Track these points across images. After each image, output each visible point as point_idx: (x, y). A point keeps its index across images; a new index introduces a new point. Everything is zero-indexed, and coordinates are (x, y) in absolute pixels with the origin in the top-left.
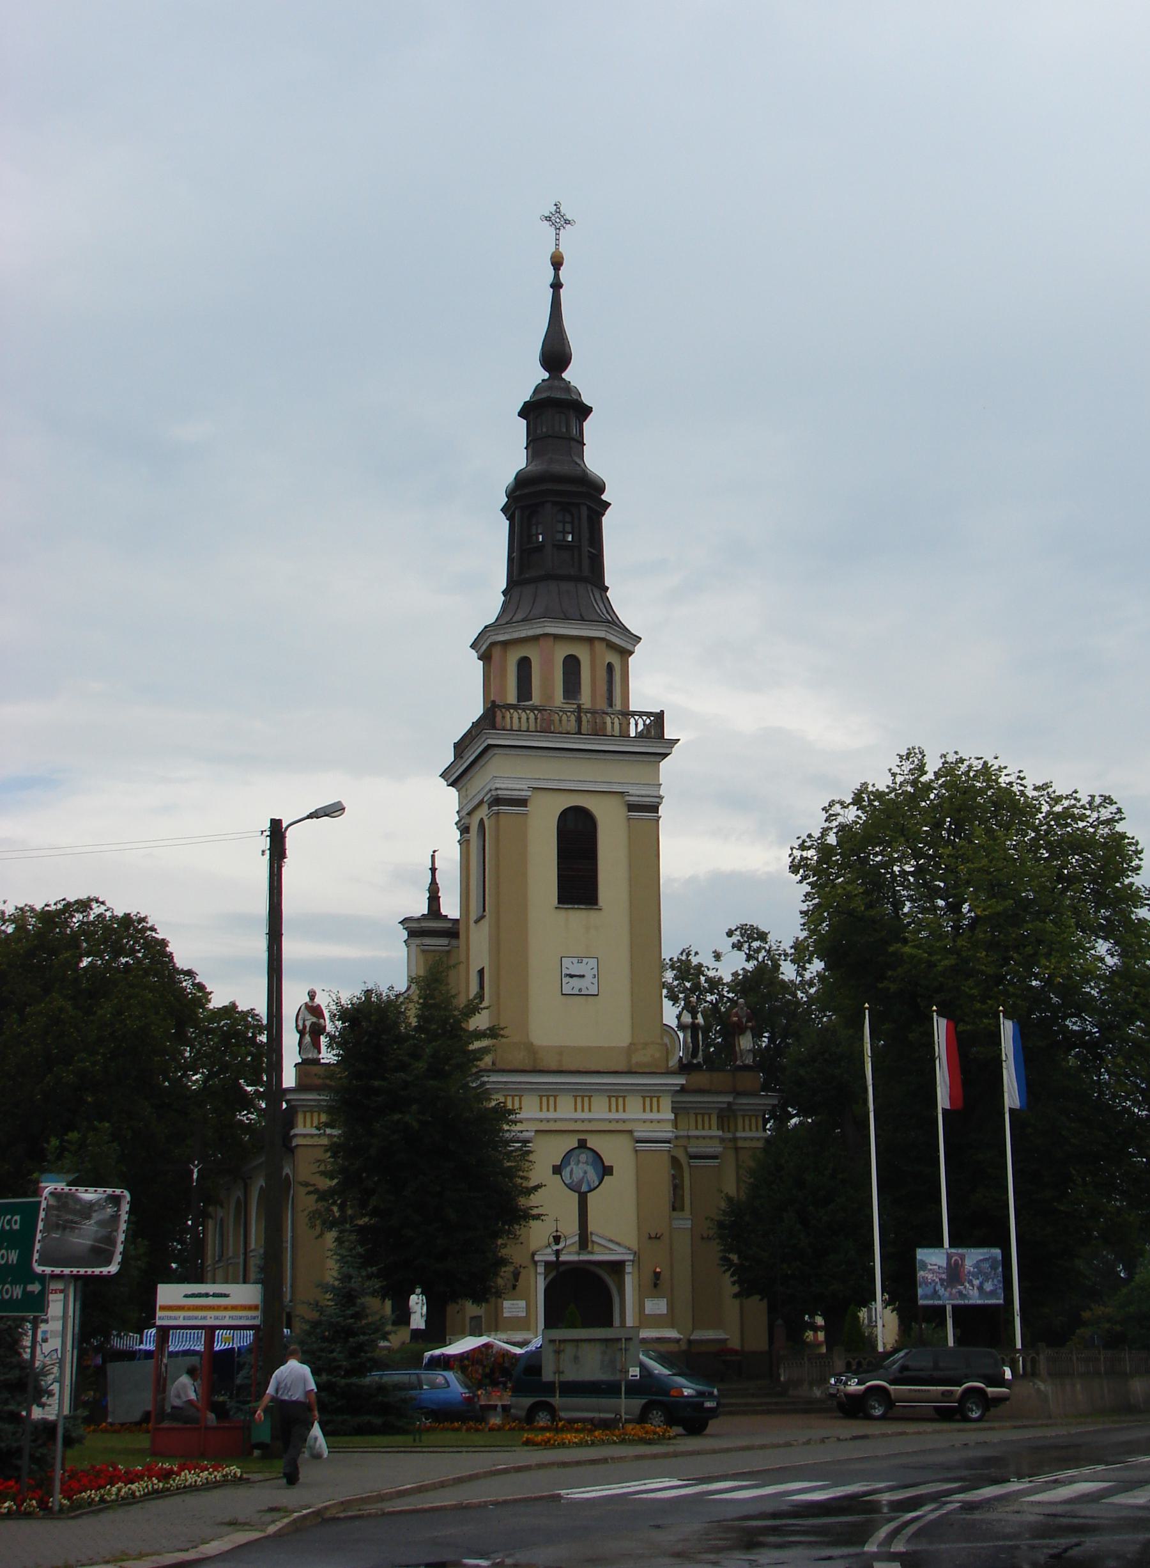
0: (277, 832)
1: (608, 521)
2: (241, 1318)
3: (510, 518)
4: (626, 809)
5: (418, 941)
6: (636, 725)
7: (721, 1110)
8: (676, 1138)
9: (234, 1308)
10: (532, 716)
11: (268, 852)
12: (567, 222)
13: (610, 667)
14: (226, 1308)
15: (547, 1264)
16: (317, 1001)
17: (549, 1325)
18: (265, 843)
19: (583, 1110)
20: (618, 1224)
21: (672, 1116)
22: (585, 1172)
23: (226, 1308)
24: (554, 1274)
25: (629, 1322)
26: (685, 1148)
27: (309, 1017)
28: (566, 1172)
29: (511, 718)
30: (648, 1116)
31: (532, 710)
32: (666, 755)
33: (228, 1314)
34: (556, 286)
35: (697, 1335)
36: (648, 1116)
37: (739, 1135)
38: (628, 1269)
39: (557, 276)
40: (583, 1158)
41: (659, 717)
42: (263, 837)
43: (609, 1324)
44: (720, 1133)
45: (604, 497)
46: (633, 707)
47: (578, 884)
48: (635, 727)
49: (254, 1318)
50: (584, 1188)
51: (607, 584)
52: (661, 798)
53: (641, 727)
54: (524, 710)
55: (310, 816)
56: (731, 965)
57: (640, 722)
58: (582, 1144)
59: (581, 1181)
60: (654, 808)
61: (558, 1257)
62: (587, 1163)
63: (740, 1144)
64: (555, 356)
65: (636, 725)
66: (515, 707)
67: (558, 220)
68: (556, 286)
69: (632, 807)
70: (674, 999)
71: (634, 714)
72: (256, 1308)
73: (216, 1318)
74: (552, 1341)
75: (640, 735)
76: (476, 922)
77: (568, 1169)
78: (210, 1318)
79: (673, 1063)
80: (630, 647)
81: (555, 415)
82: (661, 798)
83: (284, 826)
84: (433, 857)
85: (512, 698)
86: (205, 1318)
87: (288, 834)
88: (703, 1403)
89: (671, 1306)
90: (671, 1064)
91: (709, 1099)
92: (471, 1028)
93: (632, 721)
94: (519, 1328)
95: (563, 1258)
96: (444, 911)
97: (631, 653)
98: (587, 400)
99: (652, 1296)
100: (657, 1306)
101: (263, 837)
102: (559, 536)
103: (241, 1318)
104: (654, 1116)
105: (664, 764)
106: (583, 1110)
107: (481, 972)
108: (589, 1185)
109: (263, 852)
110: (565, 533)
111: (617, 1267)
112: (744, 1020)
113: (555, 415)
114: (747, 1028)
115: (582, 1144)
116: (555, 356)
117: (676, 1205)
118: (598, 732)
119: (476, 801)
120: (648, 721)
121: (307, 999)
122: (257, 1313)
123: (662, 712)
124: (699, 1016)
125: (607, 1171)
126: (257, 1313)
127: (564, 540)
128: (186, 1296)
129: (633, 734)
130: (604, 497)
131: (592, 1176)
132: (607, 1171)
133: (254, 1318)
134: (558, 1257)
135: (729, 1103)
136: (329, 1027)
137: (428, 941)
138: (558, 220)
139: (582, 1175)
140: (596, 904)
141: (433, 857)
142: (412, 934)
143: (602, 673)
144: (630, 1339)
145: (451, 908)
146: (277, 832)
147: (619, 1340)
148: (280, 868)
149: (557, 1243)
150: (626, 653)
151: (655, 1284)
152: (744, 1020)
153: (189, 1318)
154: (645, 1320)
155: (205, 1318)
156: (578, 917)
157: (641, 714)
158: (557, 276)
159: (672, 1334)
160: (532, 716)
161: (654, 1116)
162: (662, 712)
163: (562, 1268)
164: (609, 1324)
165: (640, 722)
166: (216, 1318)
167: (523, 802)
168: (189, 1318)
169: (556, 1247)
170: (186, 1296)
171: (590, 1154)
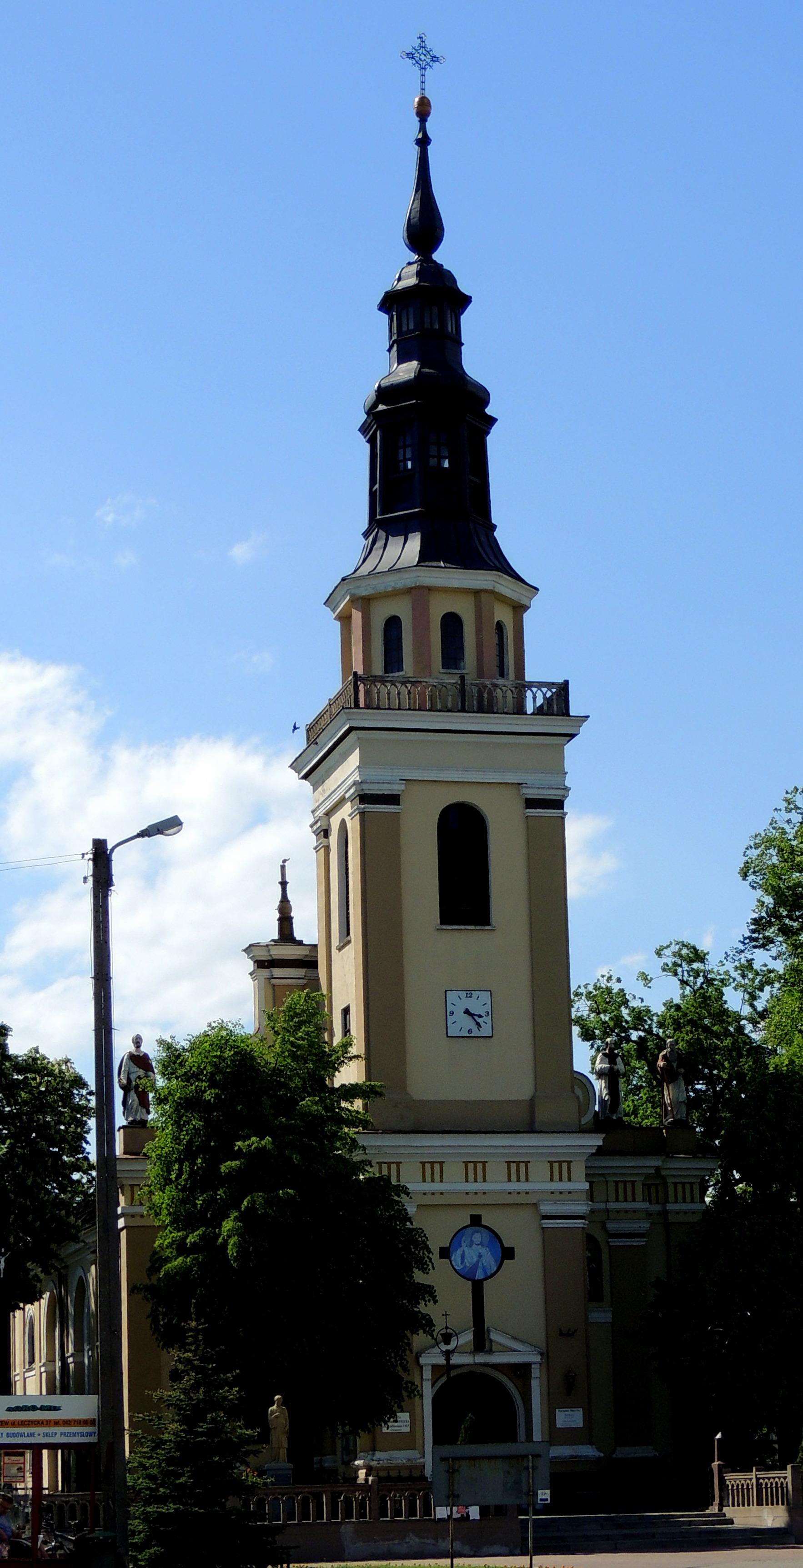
0: (101, 855)
1: (494, 441)
2: (74, 1435)
3: (372, 441)
4: (522, 804)
5: (265, 973)
6: (534, 698)
7: (648, 1176)
8: (592, 1212)
9: (67, 1423)
10: (404, 691)
11: (91, 879)
12: (435, 59)
13: (500, 627)
14: (57, 1423)
15: (435, 1367)
16: (144, 1049)
17: (438, 1440)
18: (88, 868)
19: (433, 1181)
20: (518, 1339)
21: (586, 1186)
22: (480, 1256)
23: (57, 1423)
24: (444, 1379)
25: (537, 1437)
26: (603, 1224)
27: (135, 1069)
28: (456, 1257)
29: (379, 693)
30: (556, 1186)
31: (403, 683)
32: (572, 736)
33: (59, 1430)
34: (423, 142)
35: (624, 1452)
36: (556, 1186)
37: (669, 1207)
38: (536, 1372)
39: (423, 129)
40: (477, 1238)
41: (563, 689)
42: (85, 861)
43: (513, 1439)
44: (645, 1205)
45: (489, 411)
46: (528, 678)
47: (465, 898)
48: (533, 700)
49: (91, 1434)
50: (479, 1275)
51: (494, 521)
52: (567, 789)
53: (540, 701)
54: (393, 683)
55: (143, 834)
56: (661, 994)
57: (540, 696)
58: (476, 1220)
59: (475, 1267)
60: (558, 804)
61: (448, 1359)
62: (481, 1244)
63: (672, 1218)
64: (425, 230)
65: (534, 698)
66: (383, 681)
67: (422, 57)
68: (423, 142)
69: (531, 803)
70: (588, 1035)
71: (531, 685)
72: (92, 1422)
73: (47, 1435)
74: (443, 1459)
75: (539, 711)
76: (340, 949)
77: (459, 1252)
78: (39, 1436)
79: (587, 1119)
80: (524, 601)
81: (427, 312)
82: (567, 789)
83: (109, 847)
84: (283, 868)
85: (378, 668)
86: (32, 1435)
87: (114, 856)
88: (426, 556)
89: (588, 1418)
90: (583, 1121)
91: (633, 1164)
92: (337, 1085)
93: (529, 694)
94: (409, 1435)
95: (456, 1360)
96: (298, 935)
97: (525, 608)
98: (464, 286)
99: (564, 1406)
100: (570, 1418)
101: (85, 861)
102: (433, 462)
103: (74, 1435)
104: (565, 1186)
105: (571, 749)
106: (561, 1179)
107: (346, 1011)
108: (486, 1273)
109: (85, 878)
110: (441, 458)
111: (521, 1372)
112: (675, 1065)
113: (427, 312)
114: (679, 1074)
115: (476, 1220)
116: (425, 230)
117: (594, 1294)
118: (486, 707)
119: (335, 798)
120: (549, 694)
121: (132, 1048)
122: (95, 1429)
123: (566, 683)
124: (619, 1060)
125: (508, 1253)
126: (95, 1429)
127: (440, 464)
128: (9, 1409)
129: (530, 709)
130: (489, 411)
131: (489, 1260)
132: (508, 1253)
133: (91, 1434)
134: (448, 1359)
135: (658, 1169)
136: (160, 1082)
137: (278, 972)
138: (422, 57)
139: (475, 1259)
140: (488, 924)
141: (283, 868)
142: (261, 964)
143: (491, 639)
144: (539, 1456)
145: (307, 928)
146: (101, 855)
147: (526, 1456)
148: (106, 897)
149: (447, 1342)
150: (519, 609)
151: (565, 1390)
152: (675, 1065)
153: (14, 1435)
154: (556, 1436)
155: (32, 1435)
156: (465, 940)
157: (540, 685)
158: (423, 129)
159: (588, 1451)
160: (404, 691)
161: (565, 1186)
162: (566, 683)
163: (453, 1373)
164: (513, 1439)
165: (540, 696)
166: (47, 1435)
167: (393, 799)
168: (14, 1435)
169: (444, 1348)
170: (9, 1409)
171: (486, 1234)
